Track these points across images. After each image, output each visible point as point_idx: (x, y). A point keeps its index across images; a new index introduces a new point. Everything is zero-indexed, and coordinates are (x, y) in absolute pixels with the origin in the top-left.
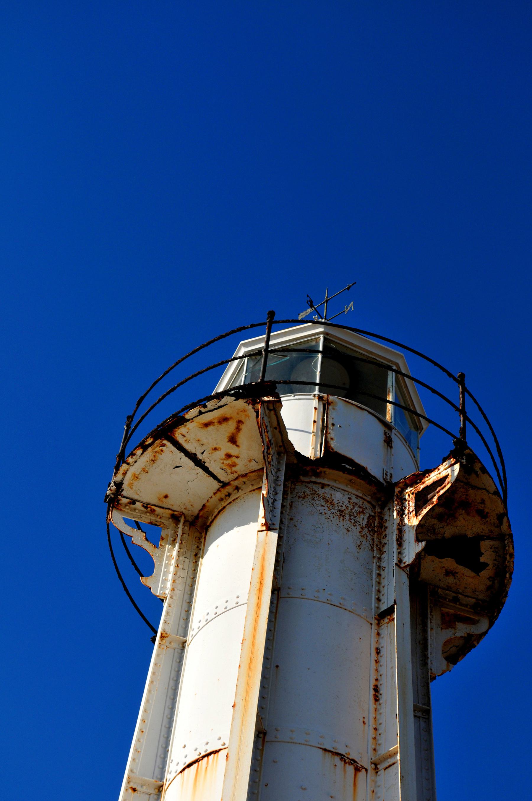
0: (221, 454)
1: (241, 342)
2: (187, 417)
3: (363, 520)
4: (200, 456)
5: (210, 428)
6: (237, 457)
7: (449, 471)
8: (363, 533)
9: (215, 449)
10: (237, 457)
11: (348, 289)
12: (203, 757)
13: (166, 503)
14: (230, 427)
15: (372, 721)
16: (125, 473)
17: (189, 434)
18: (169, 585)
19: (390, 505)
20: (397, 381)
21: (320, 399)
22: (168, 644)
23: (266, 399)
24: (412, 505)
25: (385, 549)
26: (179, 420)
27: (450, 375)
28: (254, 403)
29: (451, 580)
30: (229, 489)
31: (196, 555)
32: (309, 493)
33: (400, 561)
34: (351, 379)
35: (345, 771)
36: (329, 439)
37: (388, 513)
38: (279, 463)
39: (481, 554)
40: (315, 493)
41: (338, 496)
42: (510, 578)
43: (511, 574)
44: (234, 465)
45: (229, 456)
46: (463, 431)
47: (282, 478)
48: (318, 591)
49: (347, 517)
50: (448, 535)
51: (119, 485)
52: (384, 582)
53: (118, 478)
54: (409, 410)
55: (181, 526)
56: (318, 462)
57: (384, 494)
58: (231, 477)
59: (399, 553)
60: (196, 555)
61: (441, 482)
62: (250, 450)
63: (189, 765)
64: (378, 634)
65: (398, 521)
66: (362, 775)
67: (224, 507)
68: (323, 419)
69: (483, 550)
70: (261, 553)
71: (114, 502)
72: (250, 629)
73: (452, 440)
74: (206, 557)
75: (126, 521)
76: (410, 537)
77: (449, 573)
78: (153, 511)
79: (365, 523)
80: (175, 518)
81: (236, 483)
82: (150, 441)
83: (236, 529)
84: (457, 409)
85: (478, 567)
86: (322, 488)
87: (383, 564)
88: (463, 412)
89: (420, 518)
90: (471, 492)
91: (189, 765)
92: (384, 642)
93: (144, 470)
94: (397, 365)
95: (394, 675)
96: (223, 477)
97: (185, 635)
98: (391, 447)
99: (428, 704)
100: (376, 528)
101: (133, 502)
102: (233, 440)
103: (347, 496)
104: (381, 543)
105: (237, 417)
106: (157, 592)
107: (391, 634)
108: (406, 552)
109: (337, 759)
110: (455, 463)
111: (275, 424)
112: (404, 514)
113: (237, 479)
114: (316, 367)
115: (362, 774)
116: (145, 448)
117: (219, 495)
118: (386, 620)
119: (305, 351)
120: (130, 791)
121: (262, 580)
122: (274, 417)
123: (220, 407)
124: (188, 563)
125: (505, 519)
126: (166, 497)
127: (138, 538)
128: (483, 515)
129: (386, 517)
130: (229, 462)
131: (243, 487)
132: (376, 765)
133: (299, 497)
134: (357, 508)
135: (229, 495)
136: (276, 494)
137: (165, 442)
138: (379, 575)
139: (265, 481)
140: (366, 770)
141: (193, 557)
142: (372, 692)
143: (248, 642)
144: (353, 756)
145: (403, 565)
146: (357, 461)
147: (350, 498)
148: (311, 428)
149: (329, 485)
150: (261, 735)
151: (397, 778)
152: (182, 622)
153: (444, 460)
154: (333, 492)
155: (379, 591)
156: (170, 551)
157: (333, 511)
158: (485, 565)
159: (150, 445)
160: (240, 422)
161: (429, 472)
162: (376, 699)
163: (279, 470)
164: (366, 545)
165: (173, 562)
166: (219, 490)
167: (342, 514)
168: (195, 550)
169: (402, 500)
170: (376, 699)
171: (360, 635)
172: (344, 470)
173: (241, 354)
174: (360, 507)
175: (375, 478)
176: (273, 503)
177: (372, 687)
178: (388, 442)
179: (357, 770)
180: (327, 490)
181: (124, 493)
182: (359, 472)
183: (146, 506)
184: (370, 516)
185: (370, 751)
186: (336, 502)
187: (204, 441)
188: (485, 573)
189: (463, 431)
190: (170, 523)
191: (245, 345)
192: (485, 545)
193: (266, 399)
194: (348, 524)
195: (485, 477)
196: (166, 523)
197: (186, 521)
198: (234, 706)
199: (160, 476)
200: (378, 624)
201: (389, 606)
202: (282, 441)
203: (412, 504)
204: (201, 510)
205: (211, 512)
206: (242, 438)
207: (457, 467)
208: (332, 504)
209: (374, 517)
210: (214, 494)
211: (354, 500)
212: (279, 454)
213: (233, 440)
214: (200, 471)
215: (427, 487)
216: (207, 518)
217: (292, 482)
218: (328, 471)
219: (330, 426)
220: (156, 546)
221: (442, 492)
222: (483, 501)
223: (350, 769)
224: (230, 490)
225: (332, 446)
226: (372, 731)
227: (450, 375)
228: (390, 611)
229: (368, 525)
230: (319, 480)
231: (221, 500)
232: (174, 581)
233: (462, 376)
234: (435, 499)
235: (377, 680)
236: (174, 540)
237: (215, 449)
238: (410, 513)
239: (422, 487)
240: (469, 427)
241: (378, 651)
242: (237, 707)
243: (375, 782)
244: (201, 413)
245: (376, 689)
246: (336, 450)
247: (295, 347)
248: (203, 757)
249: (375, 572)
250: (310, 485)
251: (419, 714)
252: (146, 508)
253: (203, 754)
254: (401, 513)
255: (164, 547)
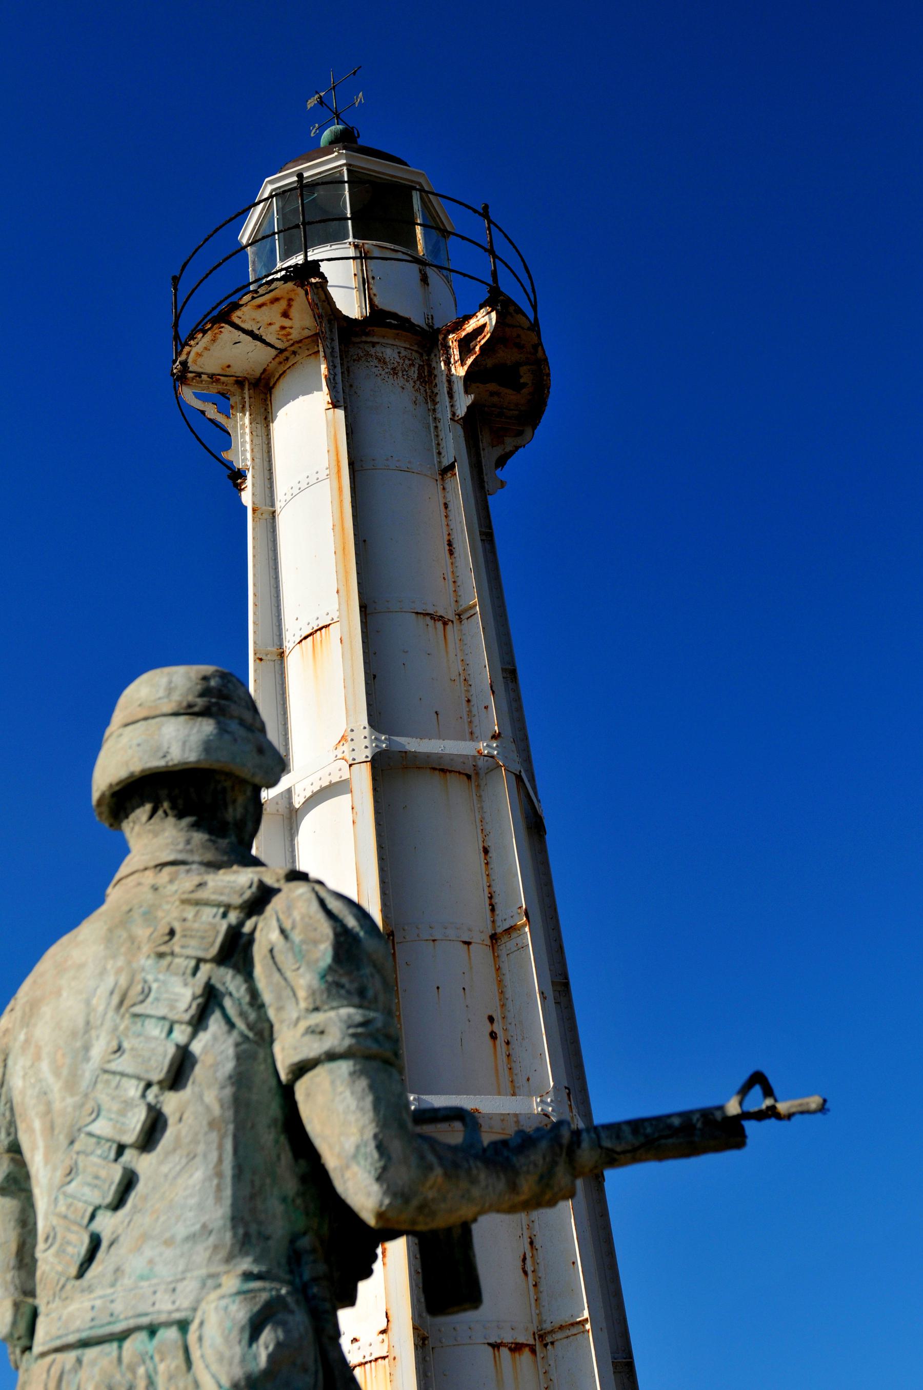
0: (276, 327)
1: (267, 180)
2: (241, 303)
3: (414, 373)
4: (257, 332)
5: (264, 308)
6: (291, 328)
7: (486, 318)
8: (417, 387)
9: (270, 324)
10: (291, 328)
11: (354, 73)
12: (316, 631)
13: (229, 372)
14: (283, 304)
15: (450, 574)
16: (189, 353)
17: (246, 316)
18: (249, 455)
19: (436, 351)
20: (422, 198)
21: (356, 247)
22: (259, 516)
23: (313, 280)
24: (456, 353)
25: (438, 399)
26: (236, 306)
27: (475, 211)
28: (302, 286)
29: (495, 399)
30: (286, 354)
31: (266, 418)
32: (362, 354)
33: (454, 414)
34: (381, 214)
35: (436, 628)
36: (372, 296)
37: (434, 360)
38: (331, 331)
39: (521, 377)
40: (368, 354)
41: (390, 354)
42: (549, 392)
43: (549, 388)
44: (289, 334)
45: (283, 328)
46: (494, 274)
47: (337, 349)
48: (387, 460)
49: (400, 374)
50: (489, 365)
51: (184, 364)
52: (442, 435)
53: (183, 357)
54: (437, 228)
55: (246, 391)
56: (366, 321)
57: (428, 341)
58: (287, 344)
59: (452, 406)
60: (266, 418)
61: (480, 330)
62: (302, 321)
63: (306, 638)
64: (444, 489)
65: (446, 372)
66: (449, 627)
67: (285, 372)
68: (362, 270)
69: (522, 374)
70: (333, 433)
71: (183, 377)
72: (337, 515)
73: (487, 288)
74: (276, 423)
75: (198, 396)
76: (459, 387)
77: (492, 394)
78: (218, 381)
79: (416, 375)
80: (240, 382)
81: (292, 348)
82: (209, 326)
83: (301, 398)
84: (486, 250)
85: (518, 387)
86: (373, 347)
87: (439, 416)
88: (491, 252)
89: (466, 368)
90: (507, 329)
91: (306, 638)
92: (450, 497)
93: (206, 349)
94: (420, 184)
95: (463, 531)
96: (279, 345)
97: (273, 505)
98: (428, 285)
99: (490, 527)
100: (427, 378)
101: (199, 375)
102: (285, 315)
103: (396, 351)
104: (433, 392)
105: (288, 296)
106: (239, 465)
107: (456, 488)
108: (457, 404)
109: (428, 618)
110: (492, 311)
111: (323, 297)
112: (450, 363)
113: (292, 345)
114: (346, 209)
115: (450, 626)
116: (205, 332)
117: (278, 360)
118: (449, 475)
119: (331, 181)
120: (258, 661)
121: (338, 461)
122: (321, 293)
123: (272, 291)
124: (260, 428)
125: (540, 348)
126: (229, 366)
127: (212, 412)
128: (520, 347)
129: (434, 364)
130: (284, 332)
131: (299, 351)
132: (459, 615)
133: (354, 360)
134: (407, 362)
135: (287, 359)
136: (335, 367)
137: (223, 325)
138: (436, 427)
139: (320, 346)
140: (452, 622)
141: (263, 421)
142: (447, 548)
143: (338, 527)
144: (441, 612)
145: (456, 418)
146: (401, 313)
147: (399, 353)
148: (353, 283)
149: (378, 343)
150: (363, 608)
151: (478, 627)
152: (267, 491)
153: (481, 309)
154: (383, 349)
155: (438, 444)
156: (242, 419)
157: (387, 370)
158: (525, 385)
159: (209, 329)
160: (290, 300)
161: (468, 318)
162: (451, 553)
163: (332, 340)
164: (421, 399)
165: (247, 430)
166: (277, 356)
167: (394, 372)
168: (264, 417)
169: (447, 348)
170: (451, 553)
171: (430, 492)
172: (390, 326)
173: (266, 195)
174: (409, 360)
175: (419, 326)
176: (334, 379)
177: (446, 543)
178: (424, 279)
179: (445, 624)
180: (378, 348)
181: (191, 369)
182: (403, 325)
183: (211, 376)
184: (420, 365)
185: (453, 603)
186: (388, 360)
187: (259, 319)
188: (525, 391)
189: (494, 274)
190: (234, 388)
191: (271, 182)
192: (523, 370)
193: (313, 280)
194: (401, 381)
195: (520, 317)
196: (232, 389)
197: (250, 384)
198: (338, 592)
199: (223, 351)
200: (443, 479)
201: (450, 462)
202: (332, 310)
203: (456, 352)
204: (262, 374)
205: (272, 375)
206: (294, 312)
207: (494, 315)
208: (385, 363)
209: (423, 366)
210: (273, 359)
211: (403, 353)
212: (330, 321)
213: (285, 315)
214: (258, 343)
215: (468, 334)
216: (269, 379)
217: (346, 347)
218: (376, 329)
219: (371, 280)
220: (228, 417)
221: (483, 342)
222: (519, 336)
223: (440, 625)
224: (287, 355)
225: (376, 303)
226: (451, 583)
227: (475, 211)
228: (451, 467)
229: (420, 377)
230: (369, 339)
231: (280, 363)
232: (252, 450)
233: (486, 207)
234: (477, 349)
235: (449, 534)
236: (244, 407)
237: (270, 324)
238: (456, 362)
239: (463, 334)
240: (501, 267)
241: (446, 506)
242: (340, 592)
243: (461, 630)
244: (253, 298)
245: (450, 544)
246: (380, 307)
247: (320, 181)
248: (316, 631)
249: (432, 425)
250: (361, 346)
251: (484, 538)
252: (211, 378)
253: (316, 628)
254: (448, 363)
255: (236, 416)
